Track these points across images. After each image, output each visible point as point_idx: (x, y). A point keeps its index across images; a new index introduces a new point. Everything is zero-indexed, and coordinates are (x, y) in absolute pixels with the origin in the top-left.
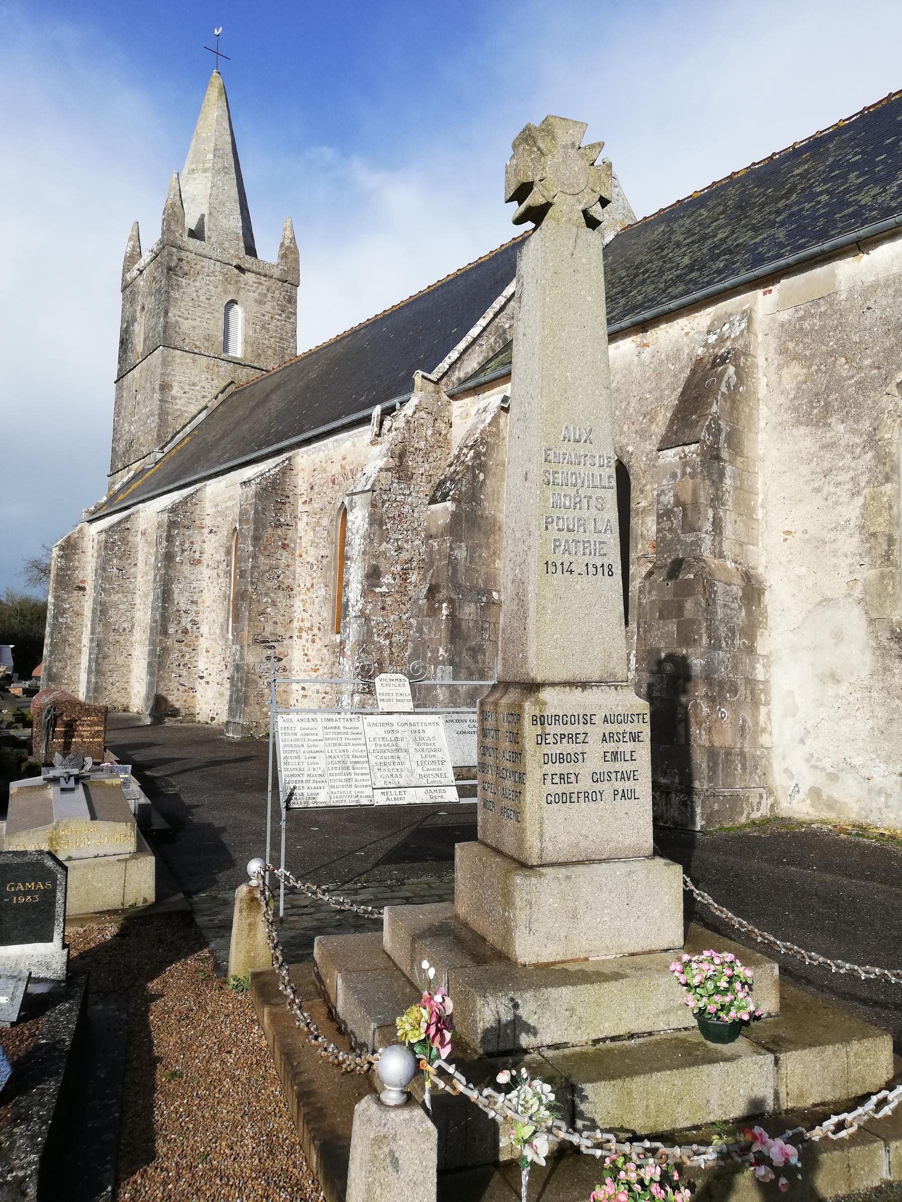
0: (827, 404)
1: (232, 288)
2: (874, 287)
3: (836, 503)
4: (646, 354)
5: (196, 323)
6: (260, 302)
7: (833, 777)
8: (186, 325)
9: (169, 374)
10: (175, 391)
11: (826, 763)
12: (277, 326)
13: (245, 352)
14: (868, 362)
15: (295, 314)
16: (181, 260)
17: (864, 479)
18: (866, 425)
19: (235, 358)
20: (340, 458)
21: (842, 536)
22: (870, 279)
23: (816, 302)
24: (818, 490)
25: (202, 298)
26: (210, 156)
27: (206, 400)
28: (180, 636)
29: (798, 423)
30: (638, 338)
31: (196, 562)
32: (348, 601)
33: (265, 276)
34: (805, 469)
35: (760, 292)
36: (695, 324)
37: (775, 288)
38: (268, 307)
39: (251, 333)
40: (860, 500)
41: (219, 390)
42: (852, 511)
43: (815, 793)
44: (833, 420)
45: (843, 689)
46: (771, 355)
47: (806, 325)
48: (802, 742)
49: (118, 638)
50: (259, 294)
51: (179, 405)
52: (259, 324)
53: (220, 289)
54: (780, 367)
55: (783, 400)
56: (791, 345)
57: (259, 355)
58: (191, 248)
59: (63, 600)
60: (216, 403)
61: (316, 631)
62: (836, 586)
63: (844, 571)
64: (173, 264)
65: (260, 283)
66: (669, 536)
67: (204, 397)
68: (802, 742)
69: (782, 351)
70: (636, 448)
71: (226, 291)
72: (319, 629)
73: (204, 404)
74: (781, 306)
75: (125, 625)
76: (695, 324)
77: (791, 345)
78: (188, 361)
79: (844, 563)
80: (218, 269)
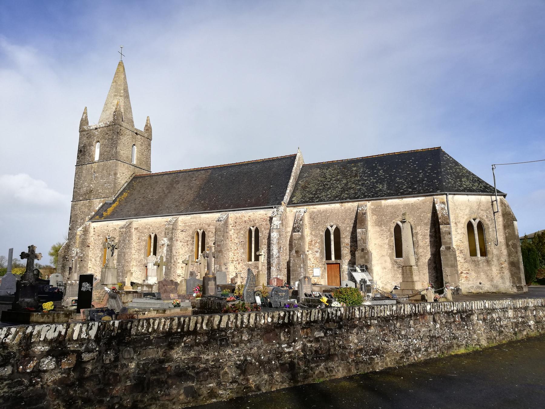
0: (381, 223)
1: (134, 140)
2: (388, 206)
3: (384, 240)
4: (343, 208)
5: (124, 152)
6: (141, 145)
7: (386, 285)
8: (122, 152)
9: (117, 170)
10: (118, 176)
11: (384, 282)
12: (146, 154)
13: (137, 162)
14: (388, 218)
15: (150, 150)
16: (121, 130)
17: (388, 237)
18: (388, 228)
19: (134, 164)
20: (248, 216)
21: (385, 245)
22: (387, 205)
23: (378, 206)
24: (381, 237)
25: (126, 143)
26: (122, 91)
27: (127, 179)
28: (174, 263)
29: (376, 226)
30: (341, 204)
31: (177, 240)
32: (273, 254)
33: (143, 136)
34: (378, 234)
35: (367, 202)
36: (354, 204)
37: (370, 202)
38: (143, 147)
39: (139, 156)
40: (388, 240)
41: (130, 175)
42: (387, 241)
43: (383, 287)
44: (383, 226)
45: (387, 270)
46: (370, 213)
47: (377, 210)
48: (380, 279)
49: (127, 264)
50: (141, 143)
51: (119, 180)
52: (141, 153)
53: (131, 140)
54: (372, 216)
55: (373, 221)
56: (374, 212)
57: (141, 164)
58: (124, 126)
59: (83, 251)
60: (130, 180)
61: (240, 261)
62: (385, 253)
63: (386, 251)
64: (119, 131)
65: (141, 139)
66: (360, 244)
67: (126, 178)
68: (380, 279)
69: (372, 213)
70: (342, 225)
71: (132, 141)
72: (241, 261)
73: (126, 180)
74: (372, 205)
75: (129, 260)
76: (354, 204)
77: (374, 212)
78: (122, 165)
79: (386, 250)
80: (130, 133)
